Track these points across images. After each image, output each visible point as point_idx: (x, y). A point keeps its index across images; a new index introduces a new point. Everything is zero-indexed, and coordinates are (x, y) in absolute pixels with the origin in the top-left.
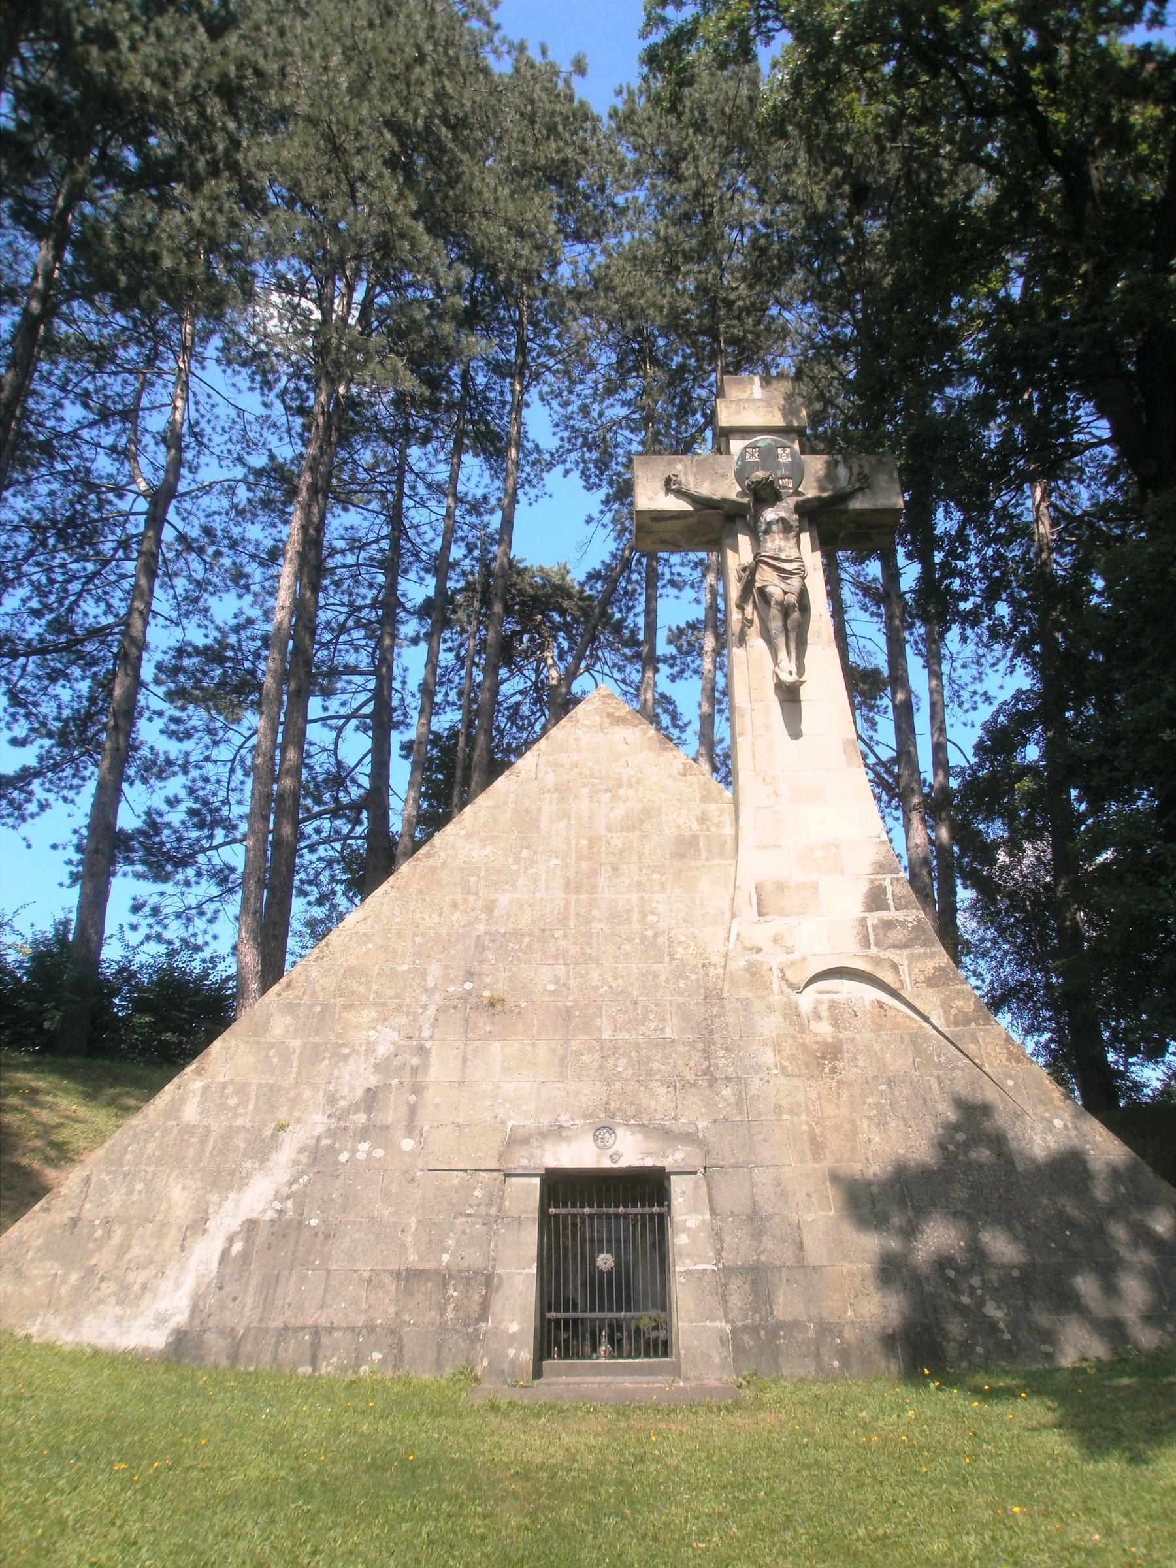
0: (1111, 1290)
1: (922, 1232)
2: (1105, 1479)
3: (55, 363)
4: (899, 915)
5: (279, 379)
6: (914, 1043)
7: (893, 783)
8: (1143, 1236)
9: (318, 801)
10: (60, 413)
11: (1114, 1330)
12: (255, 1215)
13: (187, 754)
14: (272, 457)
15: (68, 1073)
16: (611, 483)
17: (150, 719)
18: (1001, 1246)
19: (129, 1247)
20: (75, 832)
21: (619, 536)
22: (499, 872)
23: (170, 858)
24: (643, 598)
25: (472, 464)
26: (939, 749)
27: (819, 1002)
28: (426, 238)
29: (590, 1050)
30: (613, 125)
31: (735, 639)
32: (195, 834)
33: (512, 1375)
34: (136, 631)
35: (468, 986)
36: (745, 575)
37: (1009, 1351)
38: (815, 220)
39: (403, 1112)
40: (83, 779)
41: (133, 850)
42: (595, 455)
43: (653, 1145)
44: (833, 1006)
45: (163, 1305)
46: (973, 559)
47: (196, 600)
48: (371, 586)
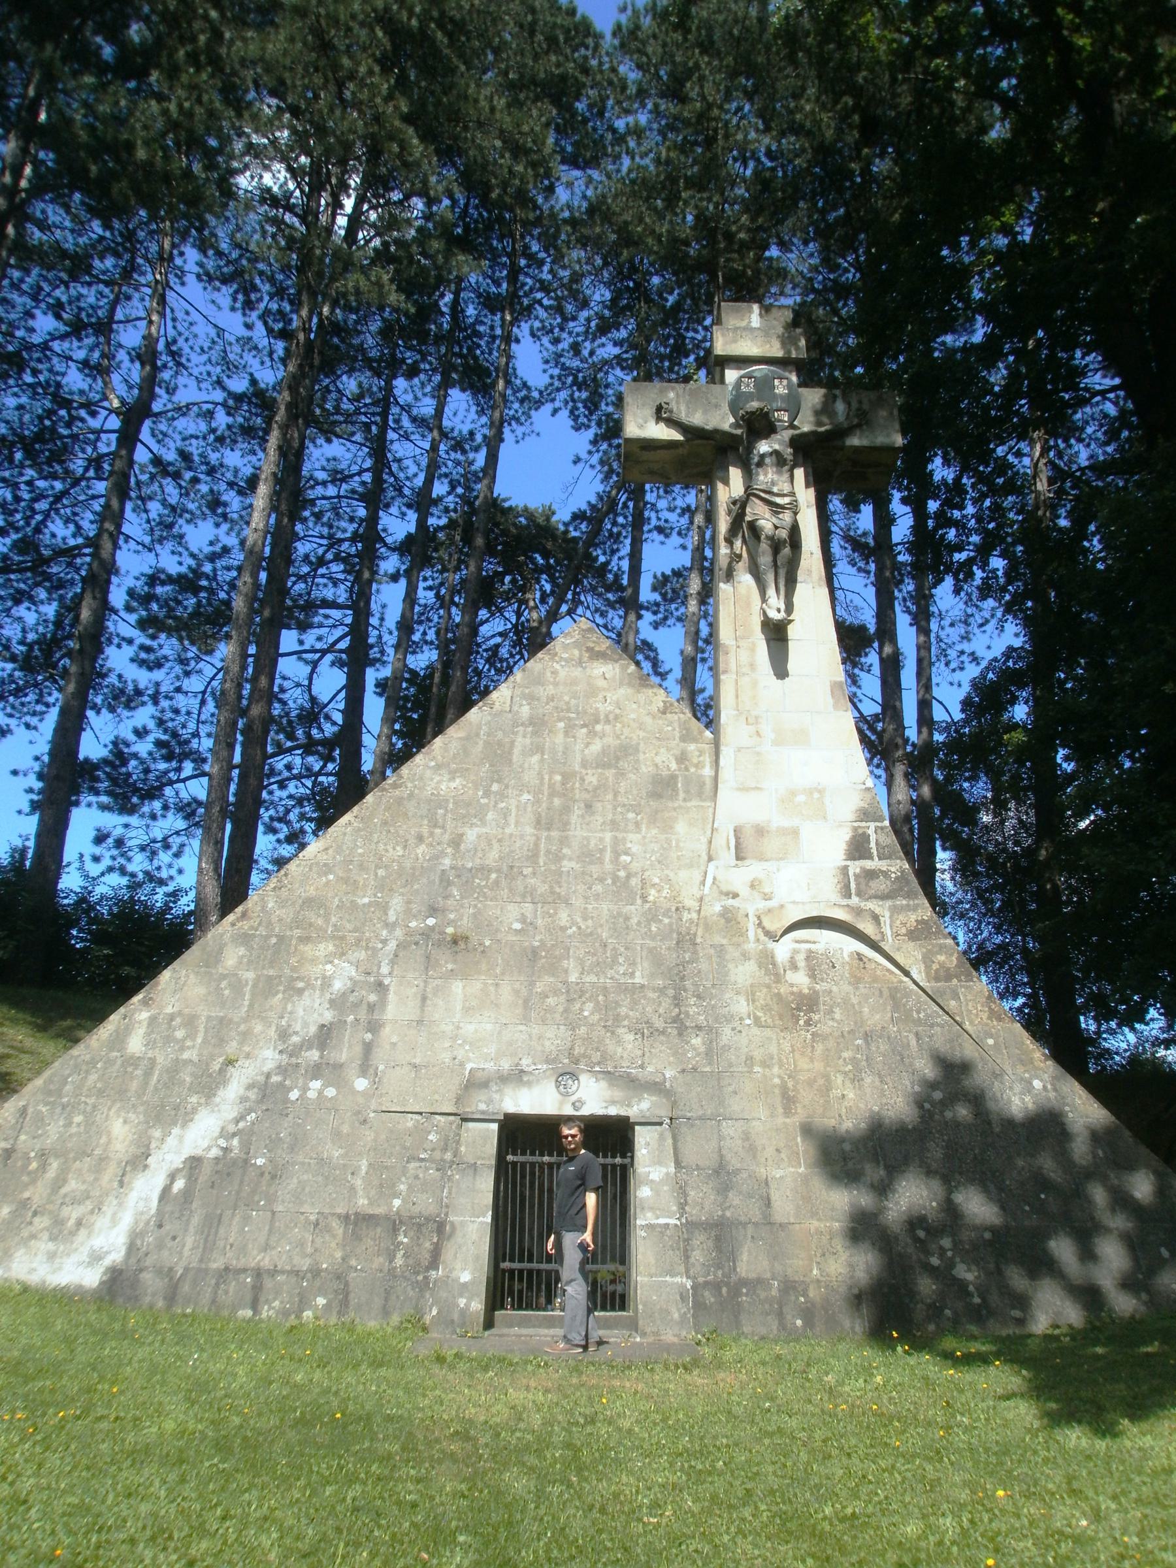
0: (1088, 1254)
1: (894, 1191)
2: (1089, 1457)
3: (27, 272)
4: (883, 865)
5: (260, 300)
6: (893, 997)
7: (879, 740)
8: (1122, 1201)
9: (291, 736)
10: (31, 323)
11: (1090, 1296)
12: (199, 1152)
13: (158, 684)
14: (254, 382)
15: (17, 1003)
16: (599, 424)
17: (119, 646)
18: (978, 1207)
19: (65, 1181)
20: (37, 759)
21: (607, 477)
22: (469, 805)
23: (136, 790)
24: (628, 541)
25: (459, 399)
26: (924, 706)
27: (796, 952)
28: (415, 141)
29: (556, 993)
30: (616, 42)
31: (722, 574)
32: (163, 766)
33: (463, 1325)
34: (105, 554)
35: (431, 922)
36: (735, 508)
37: (980, 1315)
38: (823, 152)
39: (358, 1049)
40: (47, 705)
41: (98, 780)
42: (584, 395)
43: (618, 1094)
44: (810, 956)
45: (98, 1242)
46: (970, 510)
47: (171, 526)
48: (352, 520)
